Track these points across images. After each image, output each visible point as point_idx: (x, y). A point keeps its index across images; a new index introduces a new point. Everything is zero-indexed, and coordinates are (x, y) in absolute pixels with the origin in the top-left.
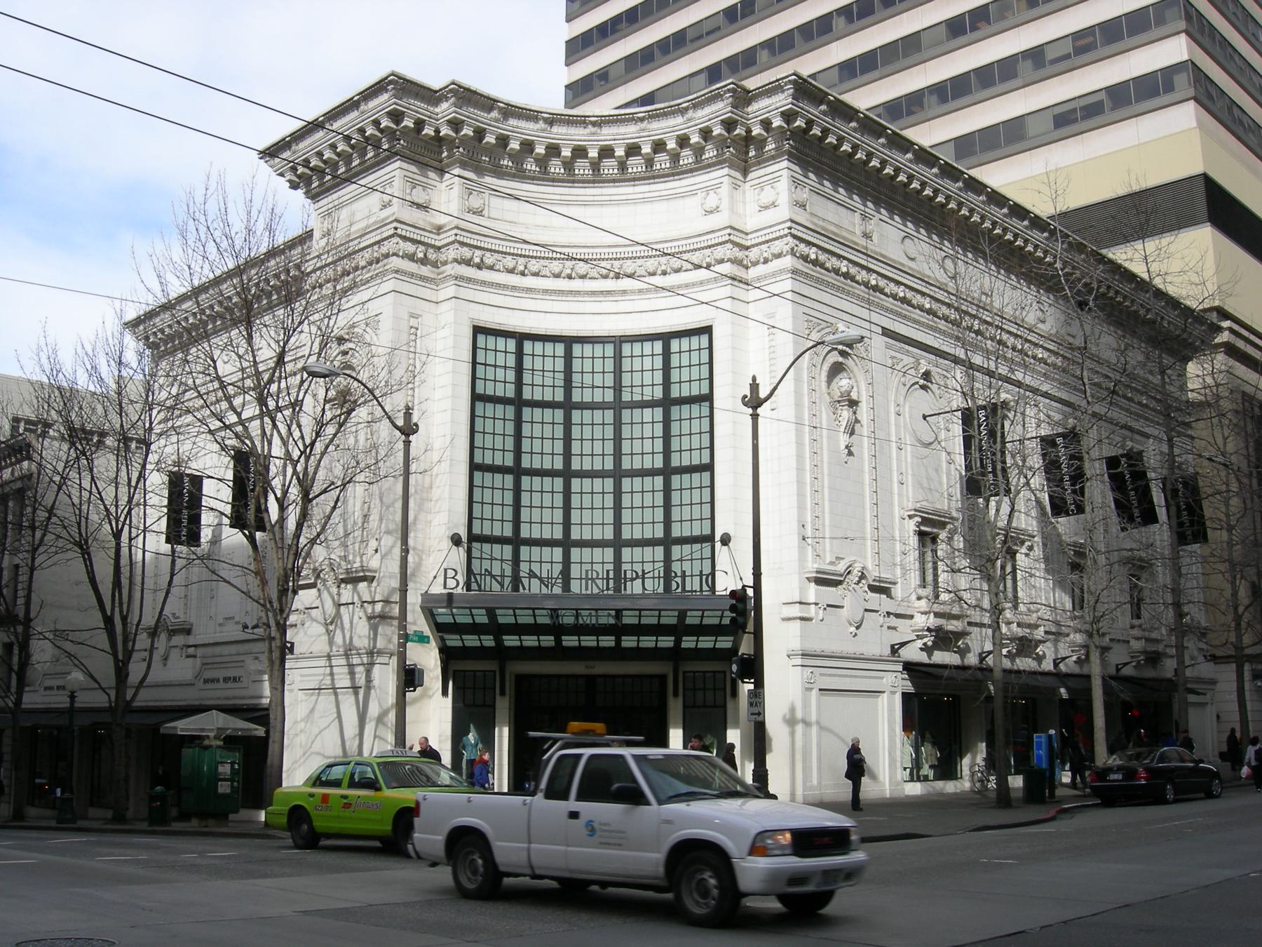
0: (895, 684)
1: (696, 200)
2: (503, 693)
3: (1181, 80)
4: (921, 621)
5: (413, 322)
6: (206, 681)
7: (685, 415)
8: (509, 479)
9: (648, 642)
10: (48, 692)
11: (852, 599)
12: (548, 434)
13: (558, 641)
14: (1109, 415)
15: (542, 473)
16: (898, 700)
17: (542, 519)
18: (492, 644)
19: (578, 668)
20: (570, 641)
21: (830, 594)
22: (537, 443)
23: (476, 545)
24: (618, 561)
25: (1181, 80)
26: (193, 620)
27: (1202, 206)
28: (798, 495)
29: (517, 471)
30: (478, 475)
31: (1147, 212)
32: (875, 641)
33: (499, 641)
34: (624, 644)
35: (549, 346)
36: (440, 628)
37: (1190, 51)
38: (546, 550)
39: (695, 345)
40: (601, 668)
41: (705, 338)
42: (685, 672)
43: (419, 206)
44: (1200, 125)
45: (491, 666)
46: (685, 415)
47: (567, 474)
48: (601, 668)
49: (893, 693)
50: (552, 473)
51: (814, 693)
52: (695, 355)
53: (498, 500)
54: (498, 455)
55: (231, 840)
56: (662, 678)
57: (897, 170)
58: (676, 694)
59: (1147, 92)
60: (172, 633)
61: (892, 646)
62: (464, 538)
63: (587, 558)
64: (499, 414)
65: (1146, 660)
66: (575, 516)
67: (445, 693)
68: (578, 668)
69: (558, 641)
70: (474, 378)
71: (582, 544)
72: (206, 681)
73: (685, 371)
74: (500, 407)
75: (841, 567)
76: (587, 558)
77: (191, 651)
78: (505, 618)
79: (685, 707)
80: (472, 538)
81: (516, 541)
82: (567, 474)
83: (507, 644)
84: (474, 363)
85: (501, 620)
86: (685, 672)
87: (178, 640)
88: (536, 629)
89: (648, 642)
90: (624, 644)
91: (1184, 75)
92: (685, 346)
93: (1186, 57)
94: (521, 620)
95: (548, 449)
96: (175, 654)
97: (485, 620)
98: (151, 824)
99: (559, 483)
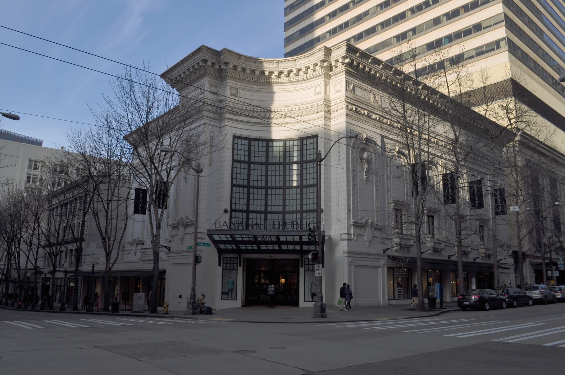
0: (383, 262)
1: (313, 89)
2: (240, 265)
3: (503, 44)
4: (396, 240)
5: (212, 134)
6: (143, 261)
7: (308, 167)
8: (246, 190)
9: (291, 247)
10: (144, 263)
11: (367, 234)
12: (260, 173)
13: (301, 247)
14: (135, 85)
15: (258, 188)
16: (386, 269)
17: (257, 204)
18: (278, 248)
19: (267, 256)
20: (284, 247)
21: (359, 231)
22: (256, 177)
23: (233, 213)
24: (284, 218)
25: (503, 44)
26: (145, 240)
27: (510, 89)
28: (347, 195)
29: (249, 187)
30: (234, 188)
31: (489, 94)
32: (378, 248)
33: (280, 247)
34: (304, 249)
35: (260, 143)
36: (216, 243)
37: (506, 33)
38: (259, 215)
39: (312, 142)
40: (276, 256)
41: (315, 139)
42: (244, 258)
43: (214, 93)
44: (510, 60)
45: (236, 255)
46: (308, 167)
47: (266, 188)
48: (276, 256)
49: (384, 267)
50: (261, 188)
51: (353, 267)
52: (312, 145)
53: (241, 197)
54: (242, 181)
55: (444, 294)
56: (298, 260)
57: (376, 72)
58: (302, 267)
59: (492, 48)
60: (137, 244)
61: (384, 250)
62: (229, 210)
63: (273, 218)
64: (242, 167)
65: (486, 256)
66: (251, 202)
67: (220, 265)
68: (267, 256)
69: (301, 247)
70: (233, 154)
71: (271, 213)
72: (143, 261)
73: (308, 151)
74: (242, 164)
75: (363, 221)
76: (273, 218)
77: (144, 250)
78: (282, 239)
79: (223, 270)
80: (232, 210)
81: (248, 212)
82: (266, 188)
83: (262, 248)
84: (233, 149)
85: (281, 240)
86: (244, 258)
87: (140, 247)
88: (272, 243)
89: (291, 247)
90: (304, 249)
91: (504, 41)
92: (308, 142)
93: (505, 35)
94: (288, 240)
95: (260, 179)
96: (138, 252)
97: (230, 239)
98: (87, 311)
99: (263, 191)
